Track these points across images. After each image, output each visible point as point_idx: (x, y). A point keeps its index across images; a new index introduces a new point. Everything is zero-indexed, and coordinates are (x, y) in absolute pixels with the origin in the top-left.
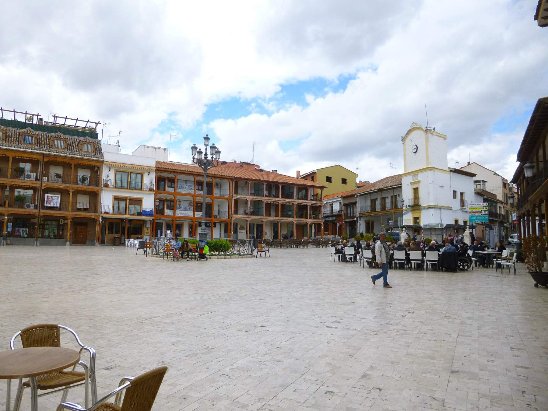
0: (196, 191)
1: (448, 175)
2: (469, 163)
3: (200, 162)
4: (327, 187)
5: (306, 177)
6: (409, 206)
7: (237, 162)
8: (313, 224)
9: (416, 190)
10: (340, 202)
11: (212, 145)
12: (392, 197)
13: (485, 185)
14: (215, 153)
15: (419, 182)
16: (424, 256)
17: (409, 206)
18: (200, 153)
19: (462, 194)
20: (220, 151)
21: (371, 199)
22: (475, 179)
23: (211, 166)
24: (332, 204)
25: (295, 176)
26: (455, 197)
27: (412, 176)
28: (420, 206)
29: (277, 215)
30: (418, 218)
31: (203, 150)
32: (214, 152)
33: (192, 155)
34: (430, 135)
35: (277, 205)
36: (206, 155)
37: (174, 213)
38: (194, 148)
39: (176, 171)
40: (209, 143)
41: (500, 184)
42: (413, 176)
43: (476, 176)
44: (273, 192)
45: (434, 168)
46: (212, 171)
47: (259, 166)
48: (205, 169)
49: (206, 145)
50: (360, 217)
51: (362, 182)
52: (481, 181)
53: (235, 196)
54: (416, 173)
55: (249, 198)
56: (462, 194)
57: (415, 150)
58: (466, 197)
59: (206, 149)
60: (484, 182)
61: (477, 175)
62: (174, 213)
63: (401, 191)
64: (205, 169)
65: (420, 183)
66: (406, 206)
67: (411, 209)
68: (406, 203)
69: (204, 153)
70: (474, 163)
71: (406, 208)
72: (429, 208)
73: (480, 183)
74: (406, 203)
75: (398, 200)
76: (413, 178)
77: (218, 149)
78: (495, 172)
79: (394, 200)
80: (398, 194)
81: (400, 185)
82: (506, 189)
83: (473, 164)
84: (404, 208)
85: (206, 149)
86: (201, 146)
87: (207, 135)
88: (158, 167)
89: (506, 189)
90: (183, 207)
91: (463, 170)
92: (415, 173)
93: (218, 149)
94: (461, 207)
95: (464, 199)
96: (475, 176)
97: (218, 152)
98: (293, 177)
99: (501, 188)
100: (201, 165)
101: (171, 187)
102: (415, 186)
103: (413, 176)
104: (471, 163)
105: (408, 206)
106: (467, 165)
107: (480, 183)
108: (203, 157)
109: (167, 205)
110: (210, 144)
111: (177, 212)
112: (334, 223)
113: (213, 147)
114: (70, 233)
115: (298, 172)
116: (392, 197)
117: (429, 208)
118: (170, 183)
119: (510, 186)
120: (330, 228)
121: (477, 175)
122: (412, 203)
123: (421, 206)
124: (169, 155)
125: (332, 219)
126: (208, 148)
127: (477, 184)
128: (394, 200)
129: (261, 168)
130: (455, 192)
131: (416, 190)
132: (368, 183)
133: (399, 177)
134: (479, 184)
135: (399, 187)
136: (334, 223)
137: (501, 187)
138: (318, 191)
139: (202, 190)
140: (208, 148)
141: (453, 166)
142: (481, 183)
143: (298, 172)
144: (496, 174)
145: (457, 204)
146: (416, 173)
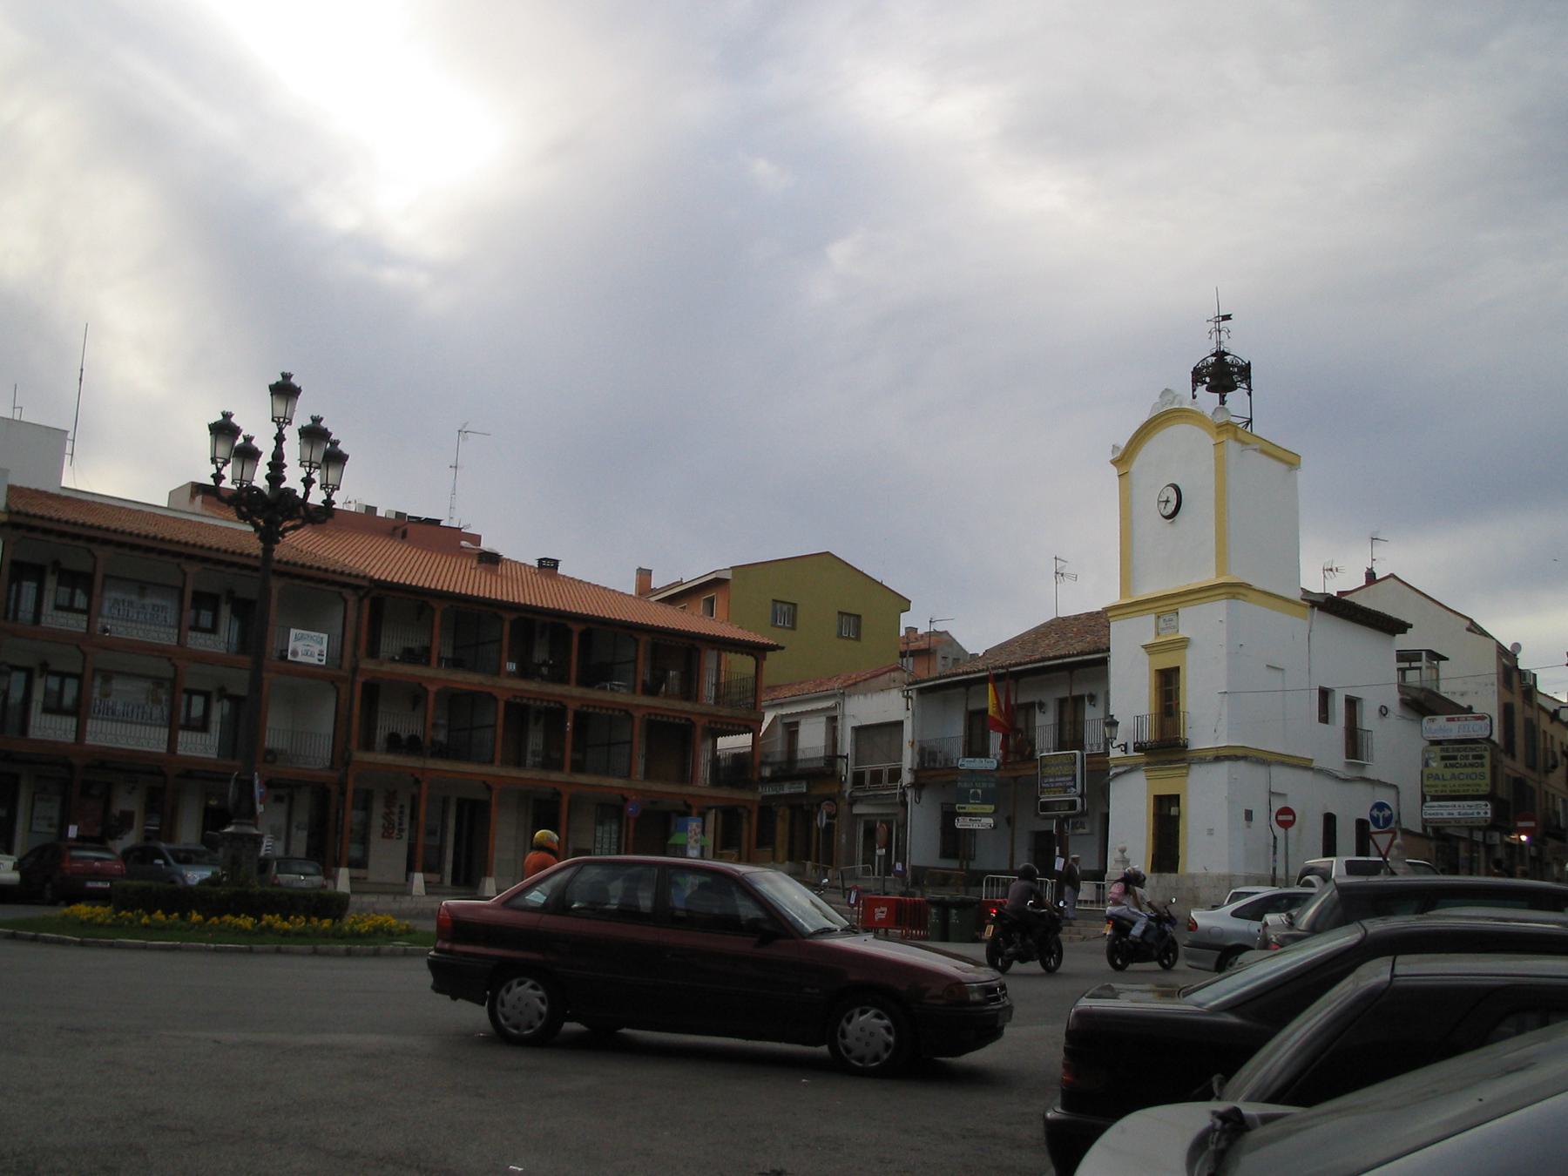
0: (190, 633)
1: (1298, 625)
2: (1371, 577)
3: (245, 502)
4: (783, 648)
5: (681, 597)
6: (1139, 747)
7: (380, 513)
8: (710, 808)
9: (1168, 682)
10: (833, 714)
11: (310, 422)
12: (1062, 702)
13: (1438, 670)
14: (320, 461)
15: (1183, 643)
16: (561, 1003)
17: (1139, 747)
18: (248, 454)
19: (1352, 703)
20: (345, 452)
21: (971, 708)
22: (1403, 642)
23: (298, 522)
24: (797, 724)
25: (631, 589)
26: (1324, 716)
27: (1153, 617)
28: (1186, 746)
29: (550, 763)
30: (1174, 799)
31: (266, 447)
32: (318, 455)
33: (214, 460)
34: (1233, 446)
35: (553, 715)
36: (277, 464)
37: (80, 731)
38: (223, 429)
39: (99, 534)
40: (293, 411)
41: (1491, 666)
42: (1159, 617)
43: (1409, 630)
44: (540, 654)
45: (1248, 587)
46: (299, 544)
47: (476, 539)
48: (269, 536)
49: (281, 422)
50: (918, 785)
51: (920, 632)
52: (1424, 654)
53: (367, 664)
54: (1172, 608)
55: (436, 676)
56: (1352, 703)
57: (1171, 507)
58: (1368, 719)
59: (280, 439)
60: (1435, 656)
61: (1411, 626)
62: (80, 731)
63: (1104, 677)
64: (269, 536)
65: (1185, 647)
66: (1126, 745)
67: (1144, 760)
68: (1124, 734)
69: (266, 458)
70: (1392, 576)
71: (1123, 754)
72: (1220, 757)
73: (1420, 660)
74: (1124, 734)
75: (1086, 718)
76: (1157, 626)
77: (335, 443)
78: (1471, 620)
79: (1068, 717)
80: (1087, 693)
81: (1103, 651)
82: (1512, 693)
83: (1388, 580)
84: (1115, 753)
85: (280, 439)
86: (257, 426)
87: (286, 377)
88: (18, 513)
89: (1512, 693)
90: (119, 708)
91: (1350, 600)
92: (1166, 605)
93: (335, 443)
94: (1347, 757)
95: (1358, 726)
96: (1404, 632)
97: (336, 458)
98: (605, 588)
99: (1495, 688)
100: (249, 510)
101: (70, 608)
102: (1166, 662)
103: (1159, 617)
104: (1377, 578)
105: (1131, 746)
106: (1364, 584)
107: (1420, 660)
108: (260, 480)
109: (47, 692)
110: (301, 418)
111: (91, 725)
112: (801, 811)
113: (314, 434)
114: (261, 793)
115: (644, 575)
116: (1062, 702)
117: (1220, 757)
118: (65, 591)
119: (1525, 679)
120: (782, 829)
121: (1411, 626)
122: (1147, 736)
123: (1191, 748)
124: (67, 459)
125: (792, 791)
126: (291, 433)
127: (1407, 665)
128: (1068, 717)
129: (485, 545)
130: (1325, 694)
131: (1168, 682)
132: (945, 637)
133: (1097, 622)
134: (1414, 664)
135: (1095, 665)
136: (801, 811)
137: (1493, 684)
138: (741, 665)
139: (213, 630)
140: (291, 433)
141: (1315, 582)
142: (1424, 663)
143: (644, 575)
144: (1474, 628)
145: (1328, 744)
146: (1172, 608)
